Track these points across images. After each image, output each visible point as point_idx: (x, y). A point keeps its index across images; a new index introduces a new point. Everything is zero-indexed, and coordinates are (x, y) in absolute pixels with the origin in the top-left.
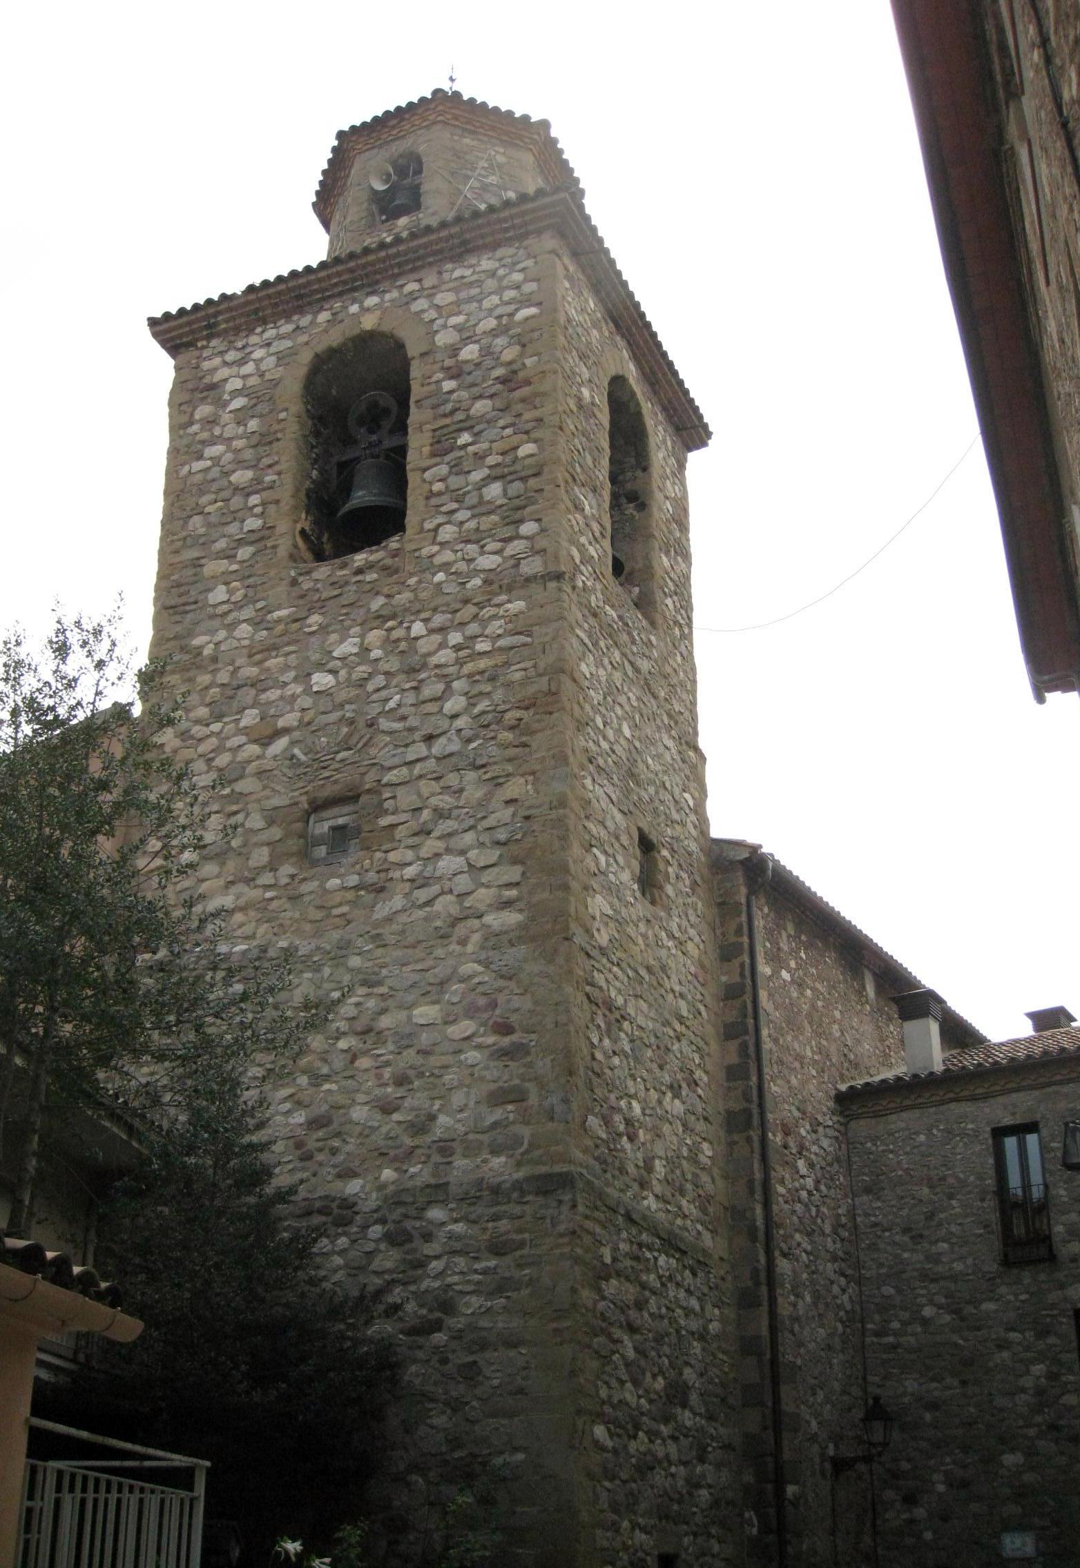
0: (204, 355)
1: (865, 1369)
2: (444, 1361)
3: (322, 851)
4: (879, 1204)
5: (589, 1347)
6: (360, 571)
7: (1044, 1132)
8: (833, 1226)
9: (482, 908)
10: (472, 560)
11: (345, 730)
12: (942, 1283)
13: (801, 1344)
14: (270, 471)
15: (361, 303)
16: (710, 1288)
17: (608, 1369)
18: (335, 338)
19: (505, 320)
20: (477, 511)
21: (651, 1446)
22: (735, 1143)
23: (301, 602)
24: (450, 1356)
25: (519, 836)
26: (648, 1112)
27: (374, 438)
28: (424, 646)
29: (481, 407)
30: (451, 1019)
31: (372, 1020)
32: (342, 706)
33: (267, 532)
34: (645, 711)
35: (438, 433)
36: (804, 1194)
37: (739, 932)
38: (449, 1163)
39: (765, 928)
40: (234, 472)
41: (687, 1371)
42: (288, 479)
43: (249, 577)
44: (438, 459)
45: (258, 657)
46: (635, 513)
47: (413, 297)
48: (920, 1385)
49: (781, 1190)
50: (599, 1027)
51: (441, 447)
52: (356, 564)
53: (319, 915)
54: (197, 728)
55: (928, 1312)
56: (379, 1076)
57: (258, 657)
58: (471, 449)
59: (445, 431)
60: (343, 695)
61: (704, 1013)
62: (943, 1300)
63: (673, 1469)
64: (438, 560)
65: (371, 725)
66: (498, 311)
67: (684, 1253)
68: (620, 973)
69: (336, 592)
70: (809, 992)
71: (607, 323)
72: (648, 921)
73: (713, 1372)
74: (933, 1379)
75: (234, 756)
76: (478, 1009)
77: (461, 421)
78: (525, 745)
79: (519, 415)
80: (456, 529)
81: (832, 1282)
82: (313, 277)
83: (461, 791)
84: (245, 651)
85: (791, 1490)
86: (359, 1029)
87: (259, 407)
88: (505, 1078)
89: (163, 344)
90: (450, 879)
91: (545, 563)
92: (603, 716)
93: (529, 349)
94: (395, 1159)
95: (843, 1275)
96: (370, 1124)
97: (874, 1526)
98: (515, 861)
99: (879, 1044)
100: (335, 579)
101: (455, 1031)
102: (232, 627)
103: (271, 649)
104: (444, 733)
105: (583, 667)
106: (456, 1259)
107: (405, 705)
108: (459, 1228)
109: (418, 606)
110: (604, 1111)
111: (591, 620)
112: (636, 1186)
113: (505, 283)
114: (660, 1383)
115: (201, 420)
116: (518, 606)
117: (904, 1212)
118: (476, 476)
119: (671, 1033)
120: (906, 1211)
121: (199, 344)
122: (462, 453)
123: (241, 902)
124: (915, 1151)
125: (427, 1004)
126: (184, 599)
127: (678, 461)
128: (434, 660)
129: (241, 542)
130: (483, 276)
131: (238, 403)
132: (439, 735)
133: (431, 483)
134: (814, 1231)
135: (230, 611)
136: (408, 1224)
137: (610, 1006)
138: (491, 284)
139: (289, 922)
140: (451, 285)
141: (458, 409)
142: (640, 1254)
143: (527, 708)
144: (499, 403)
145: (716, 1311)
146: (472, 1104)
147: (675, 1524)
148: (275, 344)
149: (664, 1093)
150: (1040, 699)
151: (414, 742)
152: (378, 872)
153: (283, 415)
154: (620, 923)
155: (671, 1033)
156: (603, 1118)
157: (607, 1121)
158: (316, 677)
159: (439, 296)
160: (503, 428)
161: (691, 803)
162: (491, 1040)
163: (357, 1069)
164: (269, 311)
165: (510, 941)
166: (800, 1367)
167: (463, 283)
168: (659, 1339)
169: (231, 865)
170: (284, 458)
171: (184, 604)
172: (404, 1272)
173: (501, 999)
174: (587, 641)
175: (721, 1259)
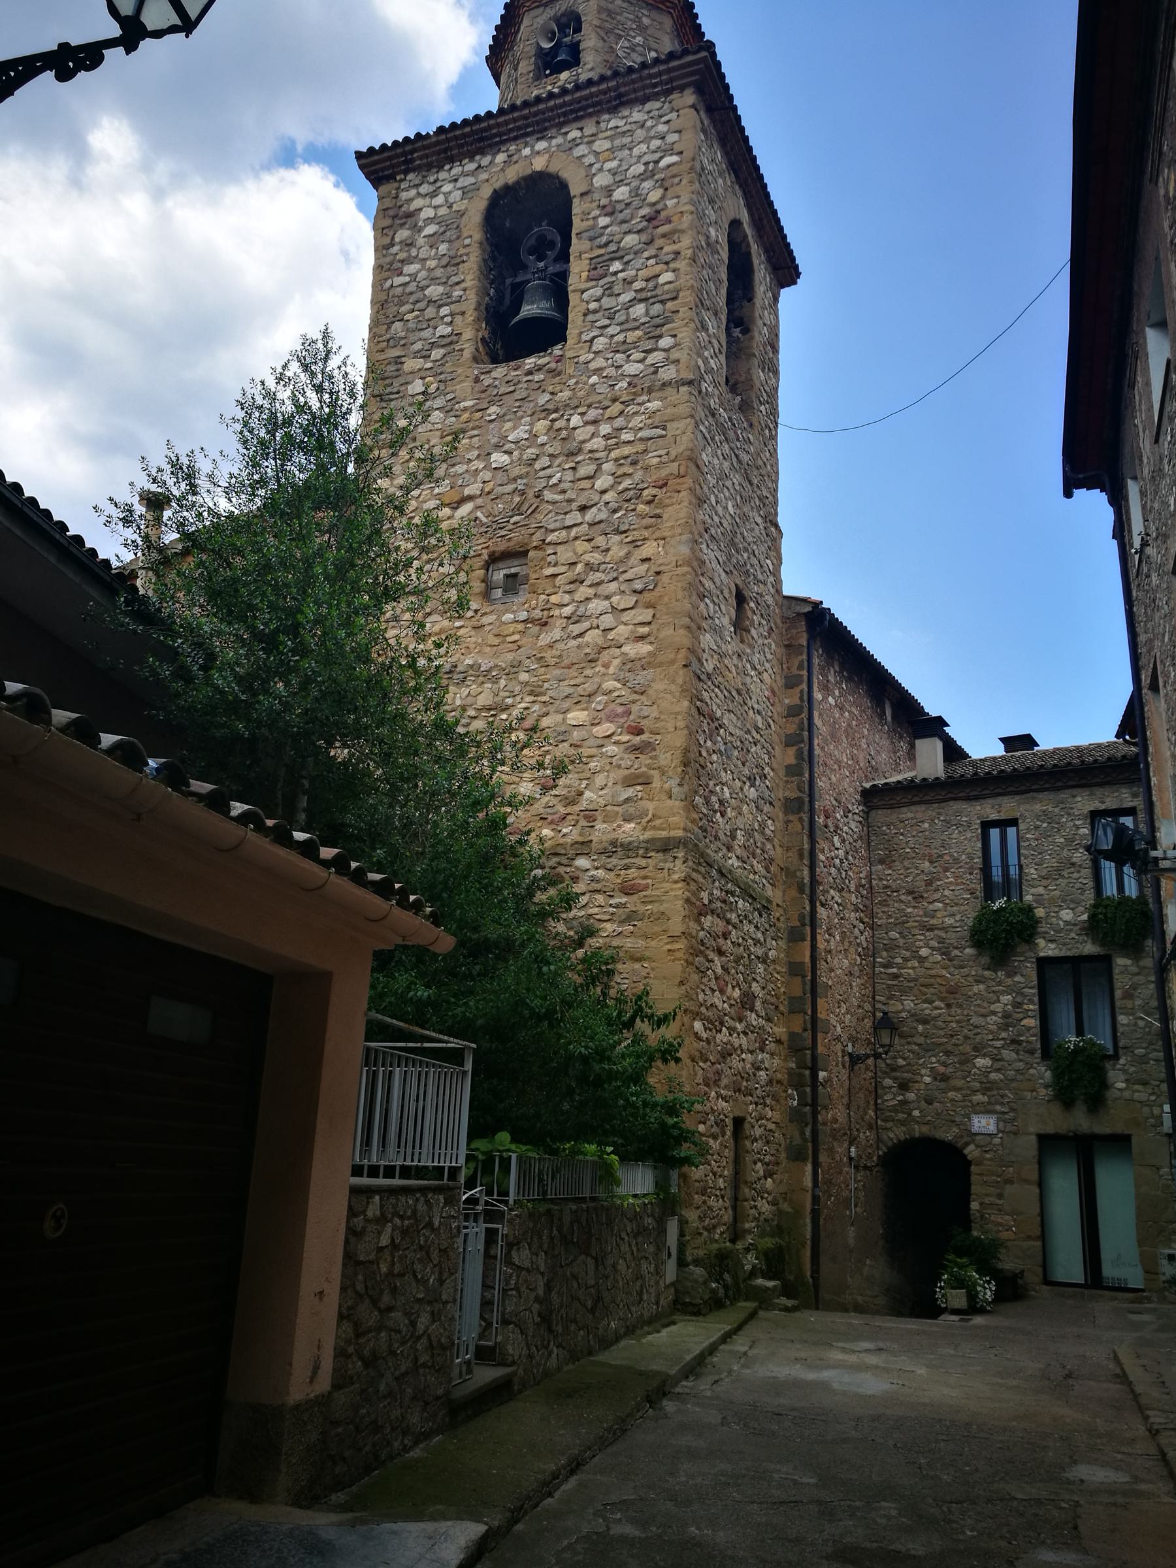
0: (402, 187)
3: (498, 593)
4: (890, 872)
5: (692, 964)
6: (530, 373)
7: (1022, 826)
9: (622, 640)
10: (621, 366)
11: (517, 499)
12: (936, 932)
13: (832, 970)
14: (457, 287)
15: (532, 147)
16: (770, 926)
17: (705, 980)
18: (512, 175)
19: (651, 166)
20: (624, 327)
23: (483, 395)
25: (651, 587)
26: (734, 796)
27: (542, 264)
28: (581, 435)
29: (630, 240)
31: (537, 720)
32: (515, 480)
33: (455, 338)
34: (744, 494)
35: (594, 261)
36: (837, 861)
37: (800, 667)
38: (593, 827)
39: (819, 665)
40: (428, 287)
41: (754, 984)
42: (472, 298)
43: (441, 374)
44: (594, 283)
46: (740, 335)
47: (575, 143)
49: (822, 857)
50: (704, 731)
51: (598, 270)
52: (527, 367)
53: (496, 641)
55: (924, 952)
58: (620, 275)
59: (600, 259)
60: (516, 472)
61: (772, 726)
62: (936, 945)
63: (744, 1056)
64: (592, 366)
65: (538, 497)
66: (646, 159)
67: (755, 899)
71: (729, 174)
72: (739, 655)
73: (770, 986)
74: (925, 1001)
77: (613, 252)
78: (659, 516)
79: (661, 248)
80: (607, 340)
82: (492, 122)
83: (608, 550)
84: (438, 433)
85: (822, 1075)
86: (527, 727)
87: (448, 233)
88: (636, 767)
90: (597, 618)
91: (677, 371)
92: (716, 496)
93: (669, 193)
94: (552, 822)
97: (876, 1104)
98: (649, 605)
100: (508, 378)
101: (600, 730)
104: (596, 504)
105: (704, 456)
106: (597, 896)
107: (565, 481)
108: (600, 873)
109: (575, 402)
110: (706, 794)
111: (710, 419)
112: (725, 850)
113: (652, 133)
114: (737, 993)
115: (401, 242)
116: (655, 405)
117: (909, 879)
118: (625, 298)
119: (751, 740)
120: (911, 878)
121: (398, 178)
122: (614, 279)
124: (920, 835)
125: (579, 710)
126: (389, 390)
127: (774, 296)
128: (588, 446)
130: (634, 126)
131: (431, 229)
132: (592, 506)
133: (588, 303)
134: (843, 889)
136: (561, 870)
137: (713, 718)
138: (640, 134)
139: (474, 646)
140: (609, 133)
141: (612, 241)
143: (661, 487)
144: (644, 237)
146: (610, 784)
148: (461, 180)
149: (745, 783)
150: (1068, 494)
151: (571, 511)
152: (542, 610)
153: (467, 241)
155: (751, 740)
156: (705, 798)
157: (707, 802)
158: (494, 457)
159: (597, 143)
160: (648, 259)
162: (625, 738)
164: (455, 152)
165: (642, 666)
167: (617, 133)
168: (738, 960)
170: (469, 277)
173: (635, 708)
174: (707, 435)
175: (778, 905)
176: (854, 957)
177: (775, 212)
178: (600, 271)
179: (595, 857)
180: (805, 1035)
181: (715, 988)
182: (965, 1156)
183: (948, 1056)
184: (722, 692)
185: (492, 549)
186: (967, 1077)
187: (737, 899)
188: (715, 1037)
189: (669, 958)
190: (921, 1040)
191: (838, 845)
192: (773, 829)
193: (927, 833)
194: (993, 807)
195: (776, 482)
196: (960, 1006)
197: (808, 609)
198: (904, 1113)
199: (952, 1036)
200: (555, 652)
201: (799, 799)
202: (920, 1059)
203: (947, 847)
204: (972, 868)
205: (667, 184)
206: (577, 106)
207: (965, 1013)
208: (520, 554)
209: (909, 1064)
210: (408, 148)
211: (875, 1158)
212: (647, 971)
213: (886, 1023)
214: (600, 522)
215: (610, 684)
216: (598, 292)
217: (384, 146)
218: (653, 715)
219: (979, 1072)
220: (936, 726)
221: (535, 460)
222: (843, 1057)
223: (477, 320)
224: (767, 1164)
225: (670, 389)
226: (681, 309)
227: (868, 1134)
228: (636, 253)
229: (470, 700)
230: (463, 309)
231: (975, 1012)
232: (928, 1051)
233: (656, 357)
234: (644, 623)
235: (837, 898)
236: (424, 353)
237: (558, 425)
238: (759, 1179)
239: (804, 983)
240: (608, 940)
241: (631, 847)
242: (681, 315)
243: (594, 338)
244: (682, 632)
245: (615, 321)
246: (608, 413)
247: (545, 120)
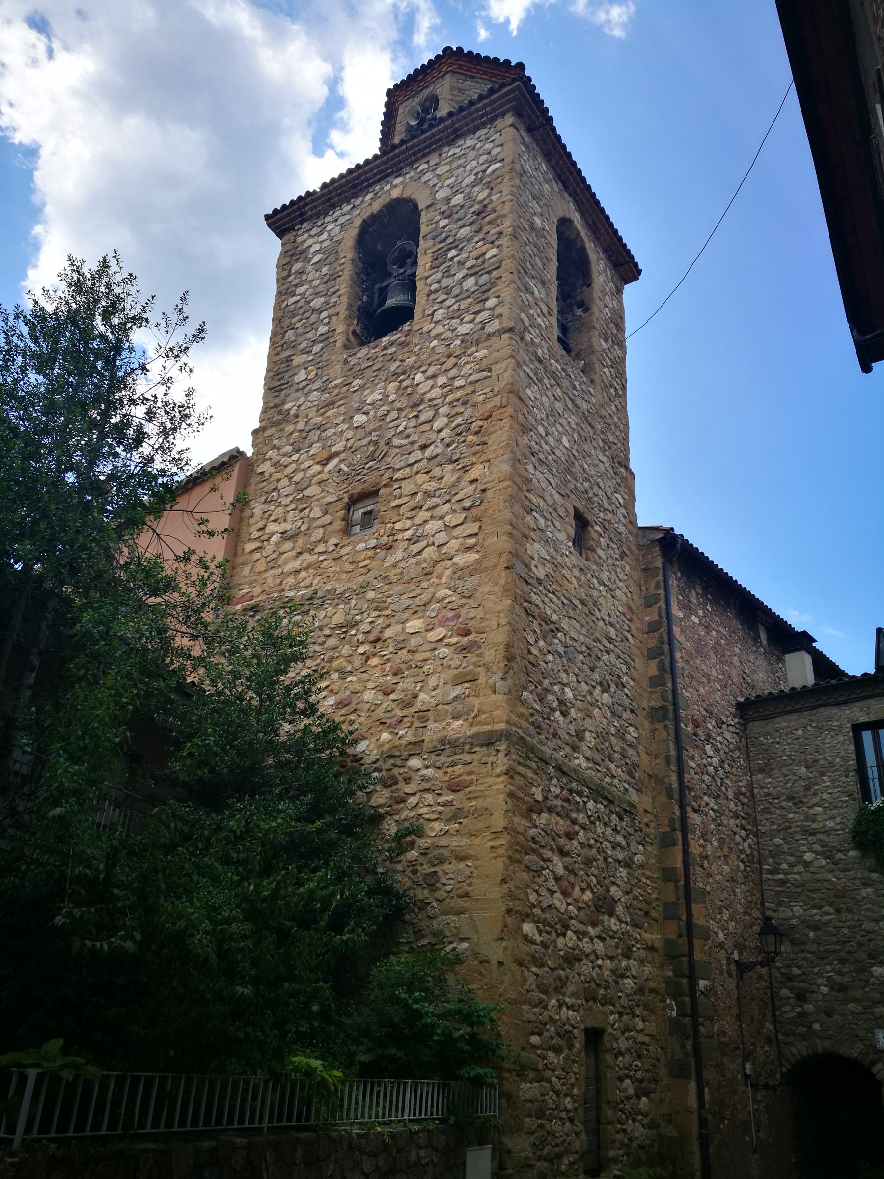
1: (763, 898)
2: (415, 872)
4: (770, 780)
6: (385, 348)
8: (735, 794)
9: (453, 553)
11: (372, 448)
12: (818, 835)
13: (709, 876)
14: (334, 296)
16: (636, 831)
17: (540, 880)
18: (376, 207)
20: (459, 298)
21: (579, 943)
22: (657, 730)
23: (349, 373)
24: (419, 868)
25: (478, 503)
27: (402, 270)
28: (422, 389)
29: (464, 232)
30: (430, 627)
31: (381, 632)
33: (331, 334)
34: (582, 433)
36: (711, 769)
37: (657, 587)
41: (613, 889)
42: (345, 300)
45: (322, 410)
47: (423, 173)
48: (805, 910)
51: (439, 259)
53: (351, 568)
54: (285, 458)
55: (808, 856)
56: (383, 670)
57: (322, 410)
58: (456, 259)
59: (440, 251)
60: (371, 427)
62: (820, 849)
63: (600, 962)
64: (433, 333)
68: (555, 599)
69: (371, 363)
70: (714, 633)
73: (637, 891)
74: (815, 907)
75: (305, 473)
76: (448, 620)
79: (488, 233)
80: (445, 311)
81: (735, 833)
82: (360, 171)
83: (442, 478)
84: (315, 408)
85: (702, 983)
88: (464, 665)
89: (274, 230)
90: (433, 536)
95: (743, 828)
96: (375, 702)
97: (774, 1015)
98: (478, 519)
99: (771, 675)
101: (433, 635)
102: (308, 394)
103: (331, 404)
108: (430, 772)
109: (419, 364)
113: (481, 151)
114: (588, 896)
116: (484, 352)
117: (788, 786)
118: (459, 276)
119: (602, 648)
122: (451, 263)
123: (305, 565)
124: (795, 742)
128: (428, 396)
129: (314, 342)
132: (431, 444)
133: (430, 286)
134: (719, 796)
135: (308, 385)
136: (396, 771)
137: (546, 620)
138: (472, 154)
139: (333, 574)
140: (448, 160)
142: (570, 798)
143: (486, 419)
144: (475, 227)
145: (641, 847)
146: (441, 684)
147: (602, 1005)
149: (594, 687)
150: (866, 368)
153: (342, 261)
154: (556, 566)
155: (602, 648)
160: (477, 243)
161: (622, 501)
163: (370, 666)
166: (709, 893)
168: (589, 862)
169: (300, 542)
171: (280, 385)
172: (391, 806)
173: (463, 611)
174: (532, 375)
175: (646, 811)
176: (736, 863)
177: (607, 218)
178: (440, 260)
179: (426, 756)
180: (680, 941)
181: (555, 888)
182: (873, 1076)
183: (843, 964)
184: (559, 598)
185: (351, 492)
186: (866, 987)
187: (585, 799)
188: (555, 941)
189: (492, 855)
190: (814, 947)
191: (710, 753)
192: (636, 735)
193: (801, 740)
194: (861, 710)
195: (627, 432)
196: (849, 911)
197: (661, 535)
198: (805, 1026)
199: (845, 943)
200: (398, 571)
201: (662, 708)
202: (815, 967)
203: (821, 751)
204: (847, 771)
205: (492, 185)
206: (423, 145)
207: (856, 917)
208: (373, 494)
209: (804, 973)
210: (301, 204)
211: (778, 1076)
212: (471, 870)
213: (768, 928)
214: (436, 456)
215: (443, 593)
216: (439, 275)
217: (284, 207)
218: (479, 616)
219: (877, 982)
220: (804, 641)
221: (386, 415)
222: (728, 964)
223: (349, 317)
224: (641, 1081)
225: (494, 338)
226: (504, 275)
227: (767, 1049)
228: (468, 241)
229: (326, 621)
230: (337, 311)
231: (866, 917)
232: (823, 959)
233: (485, 315)
234: (472, 535)
235: (712, 805)
236: (308, 350)
237: (404, 384)
238: (628, 1098)
239: (677, 888)
240: (436, 839)
241: (457, 743)
242: (504, 279)
243: (435, 311)
244: (504, 538)
245: (452, 295)
246: (444, 367)
247: (400, 162)
